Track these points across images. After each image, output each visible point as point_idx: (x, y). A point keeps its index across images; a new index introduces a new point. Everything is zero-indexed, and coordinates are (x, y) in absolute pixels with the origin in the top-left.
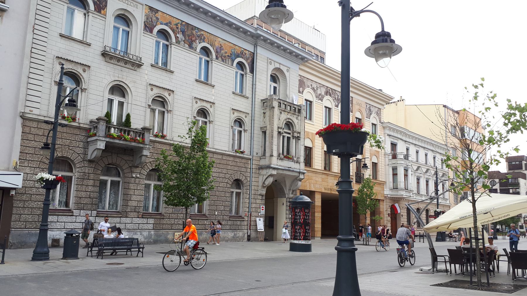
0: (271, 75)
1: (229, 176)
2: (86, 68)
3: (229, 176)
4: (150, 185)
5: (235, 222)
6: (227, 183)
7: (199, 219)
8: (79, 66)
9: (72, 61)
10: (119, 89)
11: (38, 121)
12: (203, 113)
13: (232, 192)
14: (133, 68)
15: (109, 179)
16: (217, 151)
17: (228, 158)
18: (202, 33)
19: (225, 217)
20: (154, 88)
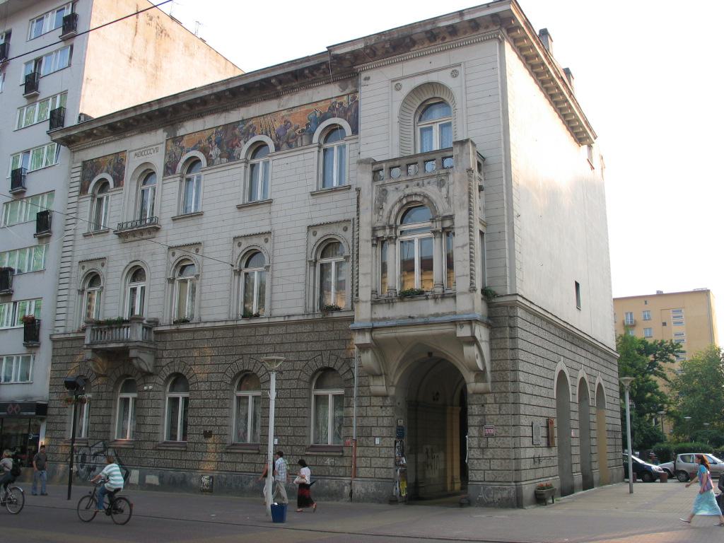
0: (267, 145)
1: (302, 364)
2: (197, 247)
3: (302, 364)
4: (128, 399)
5: (319, 459)
6: (298, 379)
7: (242, 453)
8: (334, 226)
9: (250, 235)
10: (137, 273)
11: (213, 329)
12: (251, 255)
13: (127, 400)
14: (136, 238)
15: (250, 394)
16: (217, 324)
17: (300, 329)
18: (251, 123)
19: (295, 449)
20: (85, 264)
